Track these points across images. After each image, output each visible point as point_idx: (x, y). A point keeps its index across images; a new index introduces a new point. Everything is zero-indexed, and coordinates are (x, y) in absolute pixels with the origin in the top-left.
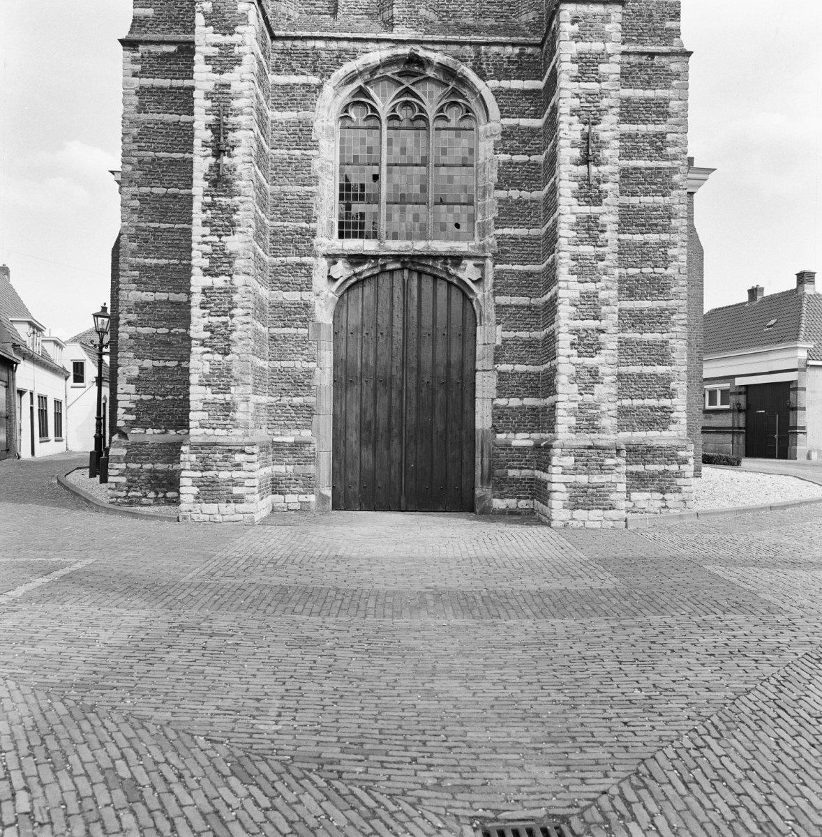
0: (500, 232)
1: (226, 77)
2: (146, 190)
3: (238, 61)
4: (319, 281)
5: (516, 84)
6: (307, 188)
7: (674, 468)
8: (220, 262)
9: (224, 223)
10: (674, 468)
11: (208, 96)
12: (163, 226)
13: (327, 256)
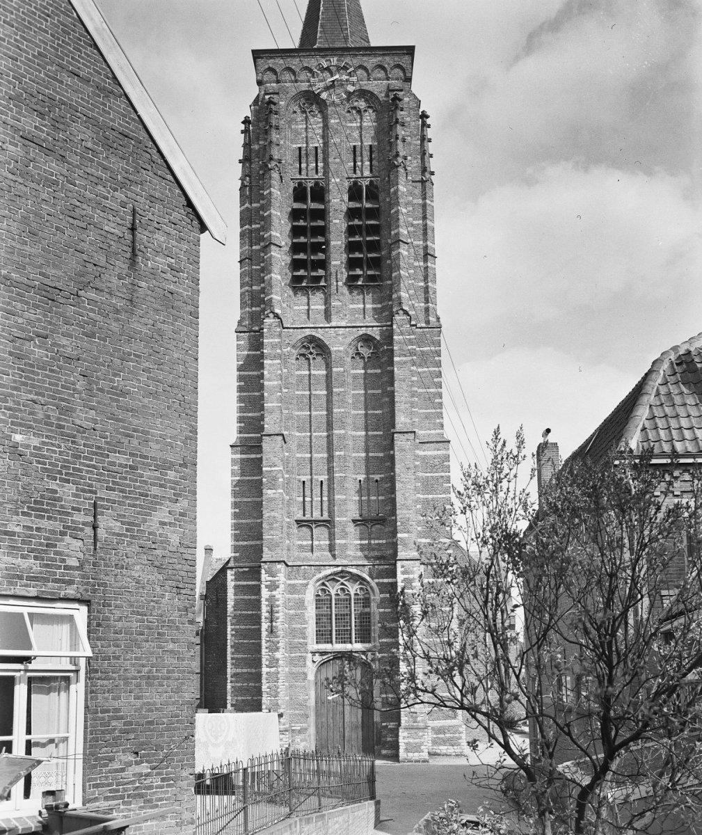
0: (380, 641)
1: (274, 593)
2: (238, 627)
3: (278, 587)
4: (309, 663)
5: (386, 581)
6: (303, 626)
7: (457, 735)
8: (274, 662)
9: (274, 648)
10: (457, 735)
11: (267, 600)
12: (245, 641)
13: (312, 653)
